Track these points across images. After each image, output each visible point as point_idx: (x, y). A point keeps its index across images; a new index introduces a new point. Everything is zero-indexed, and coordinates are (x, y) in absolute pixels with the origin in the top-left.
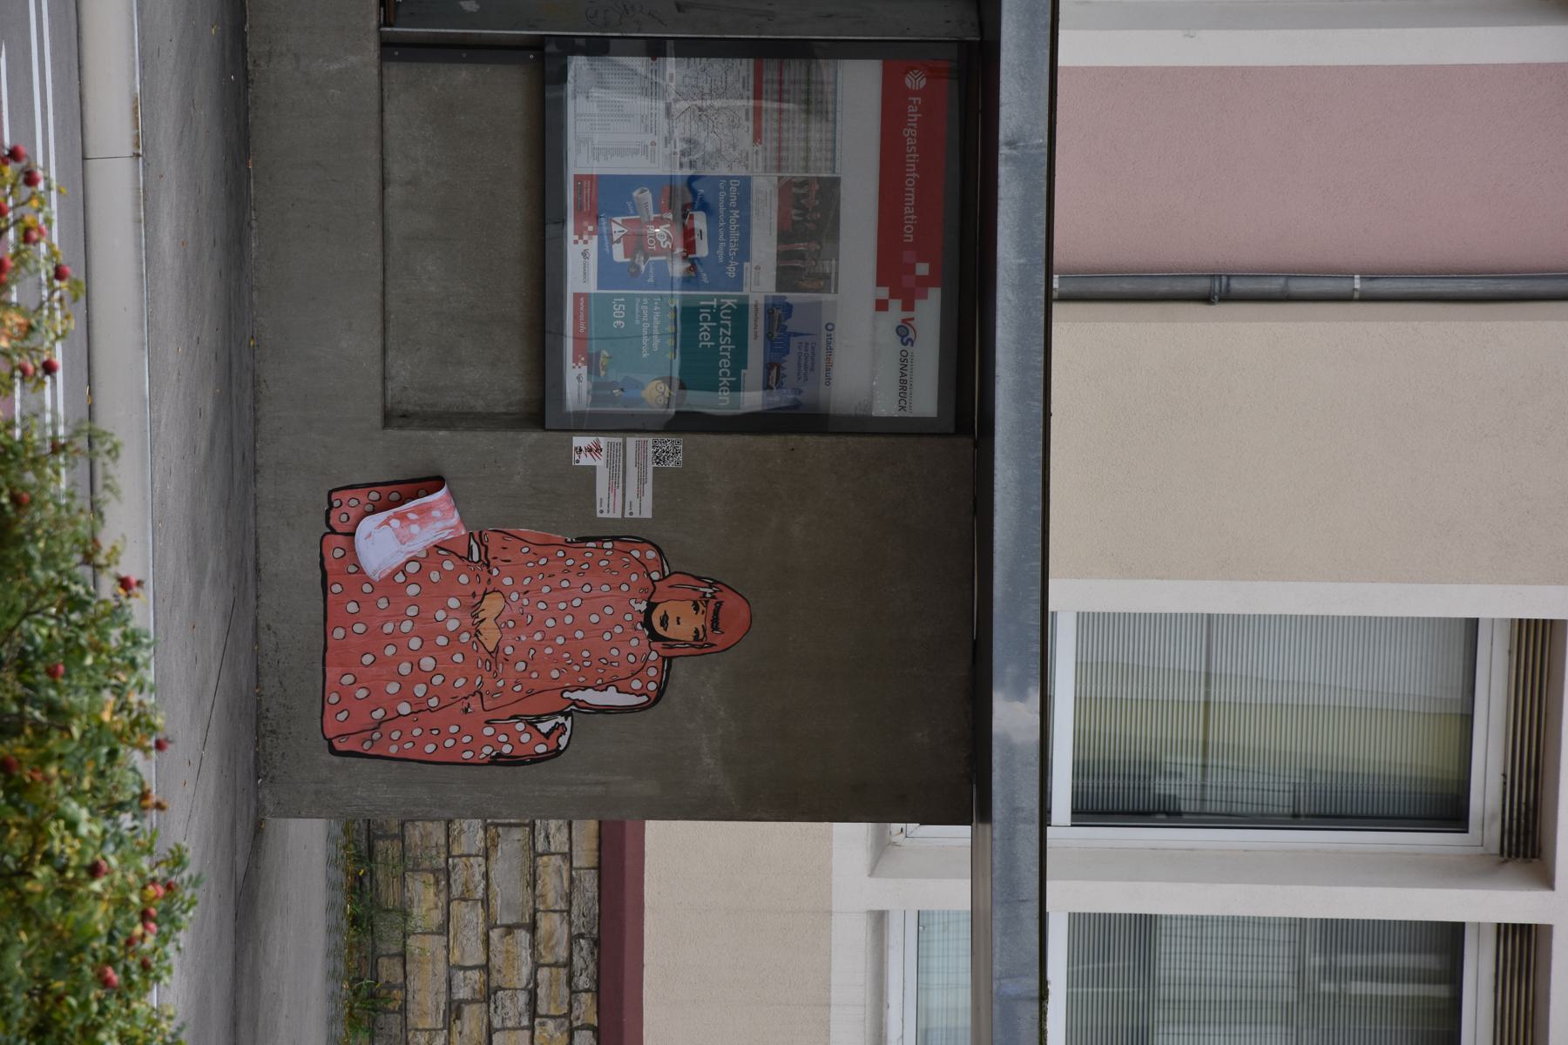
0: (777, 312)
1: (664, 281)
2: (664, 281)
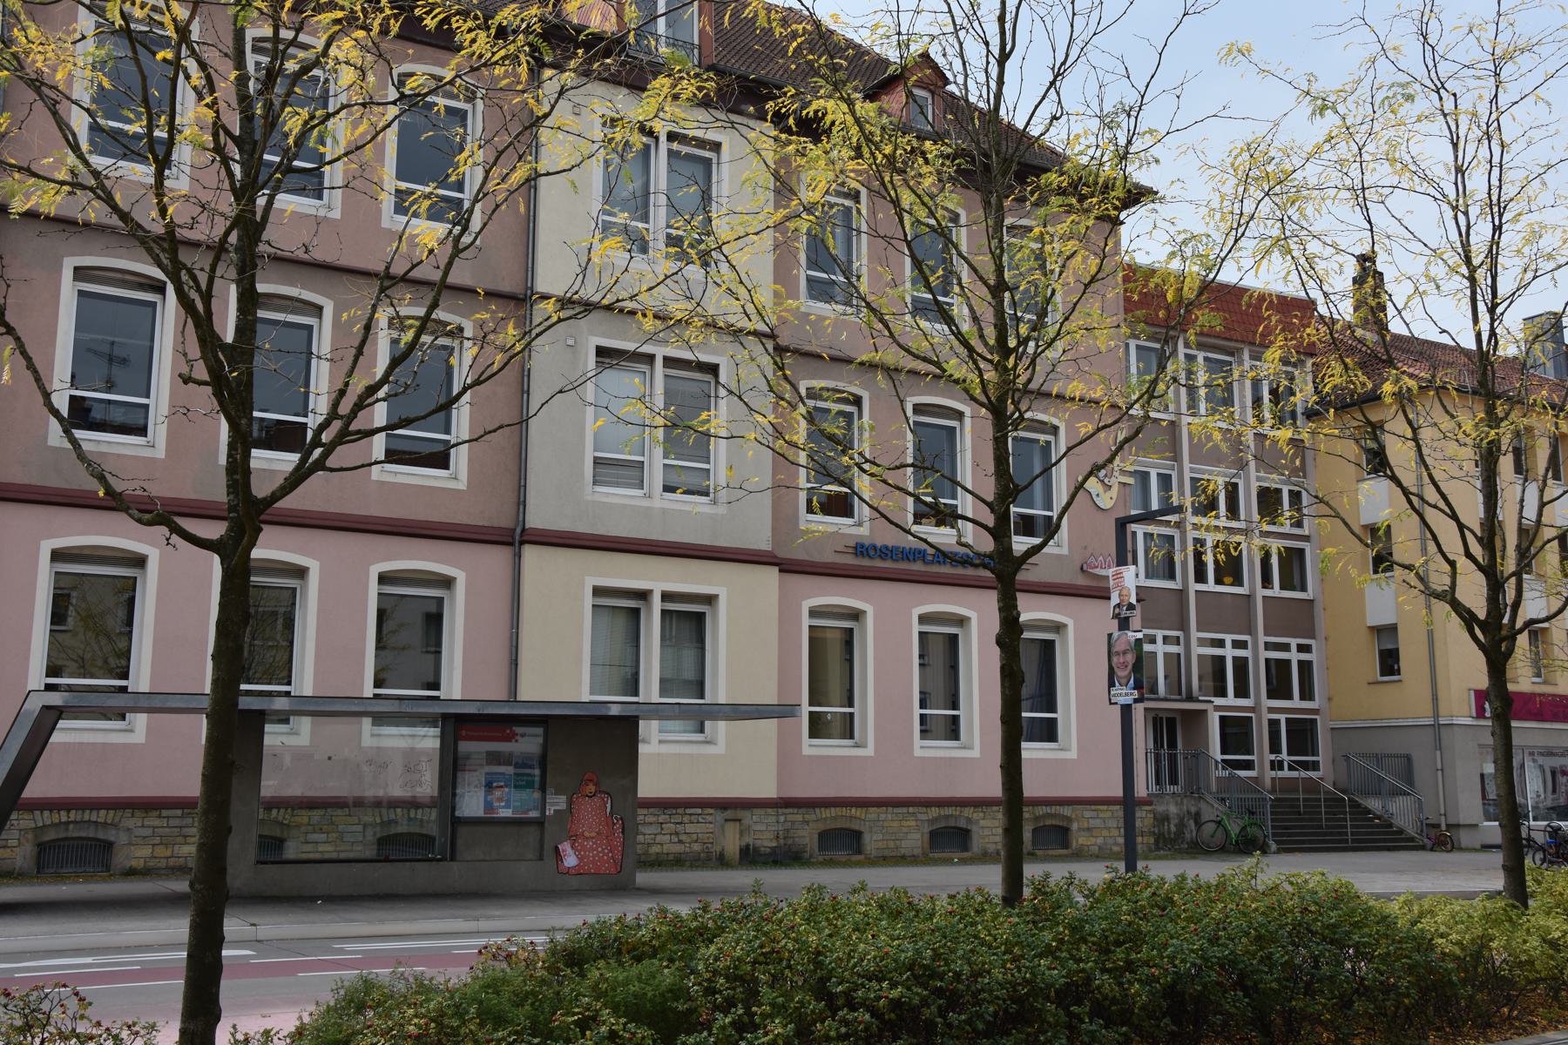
0: (517, 766)
1: (509, 793)
2: (509, 793)
